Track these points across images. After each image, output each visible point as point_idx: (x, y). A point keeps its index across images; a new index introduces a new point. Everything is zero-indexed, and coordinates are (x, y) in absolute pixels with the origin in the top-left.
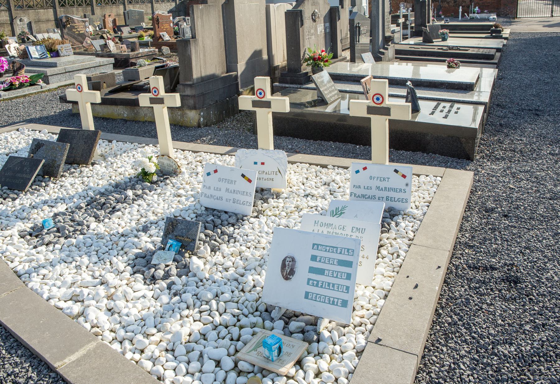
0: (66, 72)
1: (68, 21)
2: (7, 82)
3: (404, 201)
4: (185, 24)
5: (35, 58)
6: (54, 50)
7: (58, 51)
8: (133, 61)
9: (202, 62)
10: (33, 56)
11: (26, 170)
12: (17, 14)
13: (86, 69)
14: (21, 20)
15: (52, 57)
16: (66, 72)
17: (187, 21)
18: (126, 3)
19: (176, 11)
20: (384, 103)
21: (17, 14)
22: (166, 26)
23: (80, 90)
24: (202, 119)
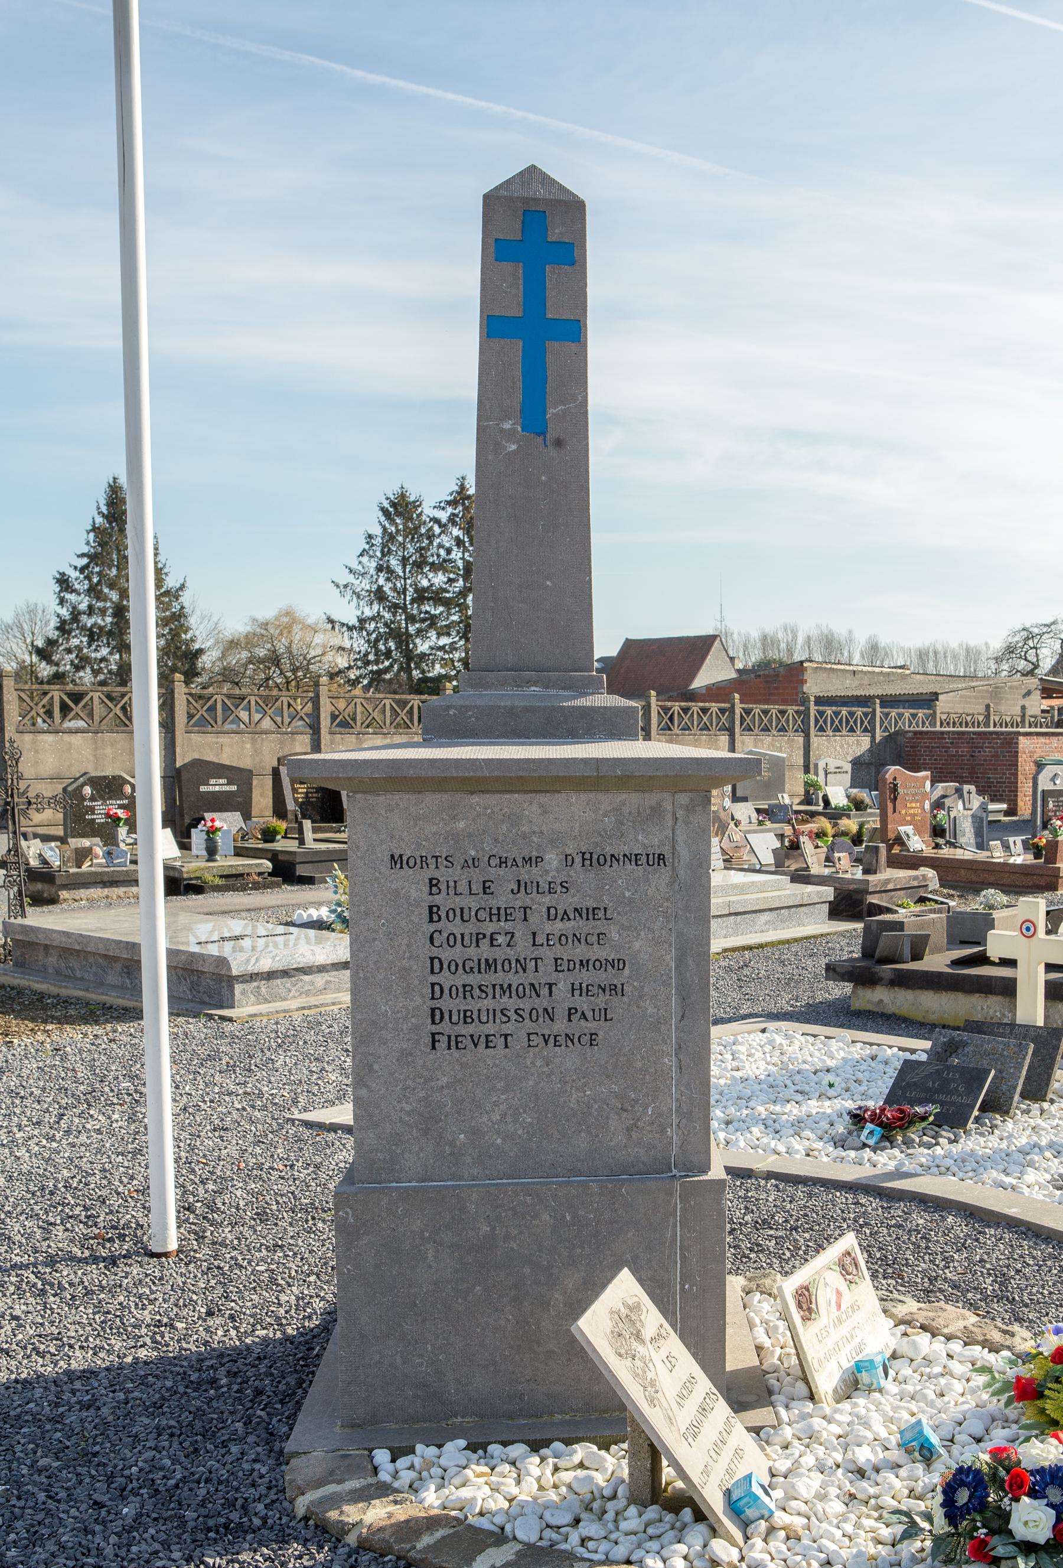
0: (730, 914)
4: (960, 806)
8: (874, 900)
11: (956, 1089)
13: (771, 910)
16: (730, 914)
17: (966, 795)
18: (737, 730)
19: (870, 764)
22: (914, 808)
23: (1030, 933)
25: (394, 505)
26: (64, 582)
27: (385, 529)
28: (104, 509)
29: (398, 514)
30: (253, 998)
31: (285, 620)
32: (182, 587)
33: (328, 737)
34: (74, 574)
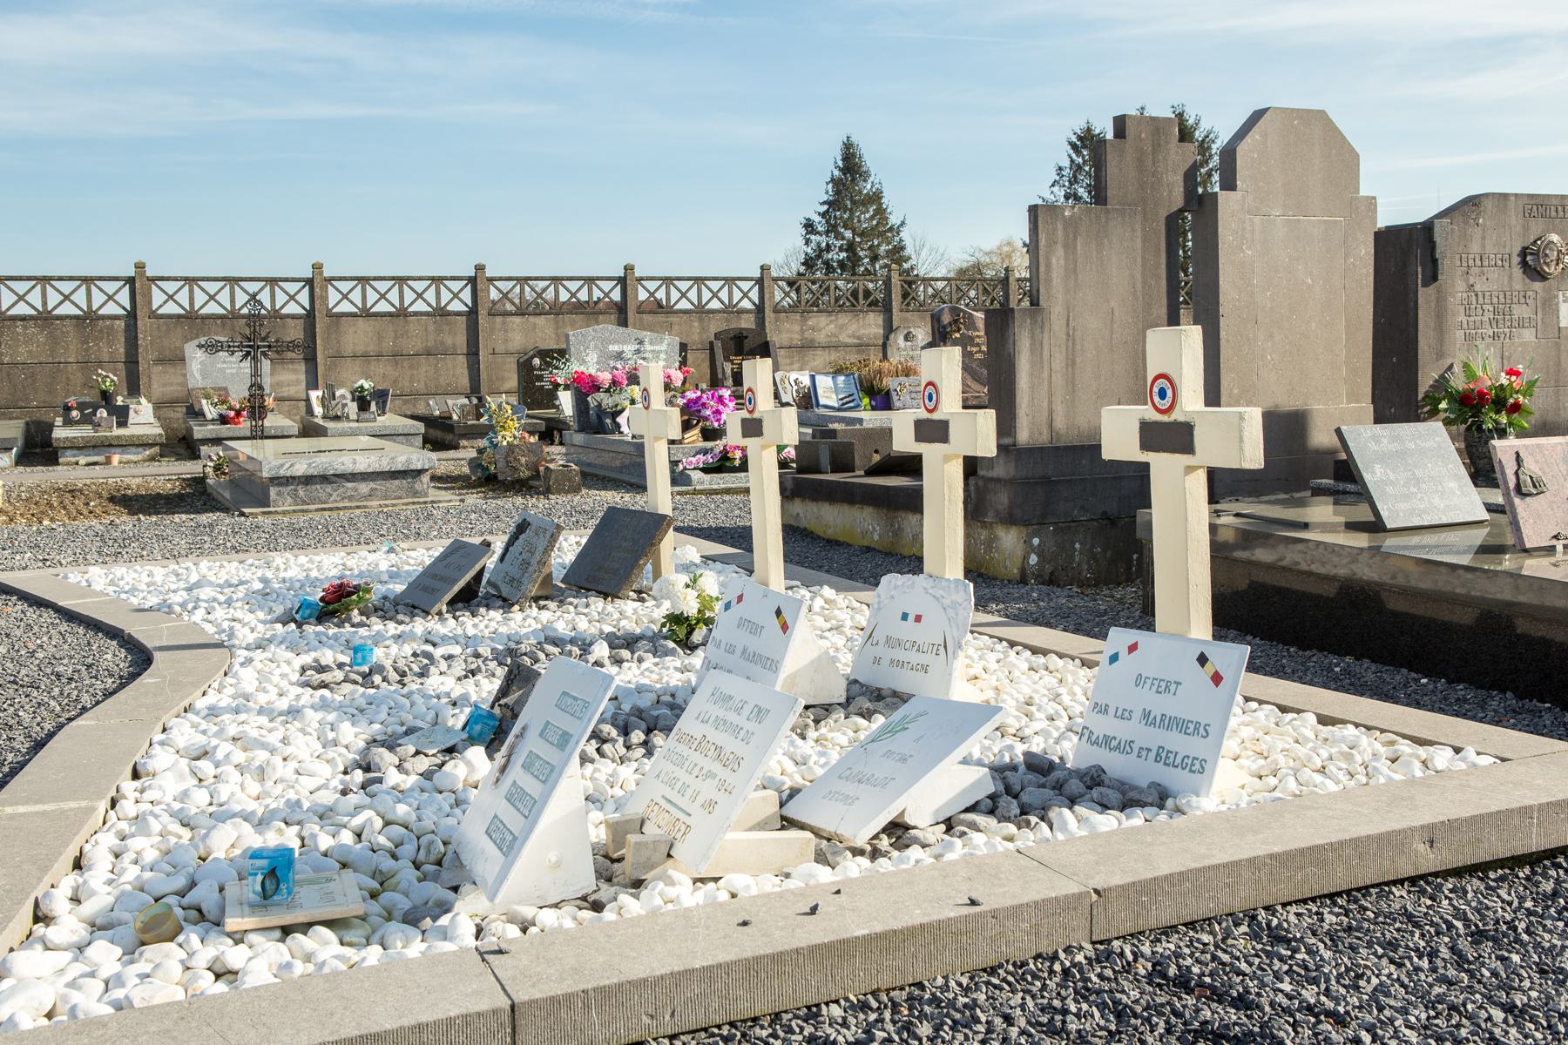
1: (956, 321)
2: (717, 451)
3: (1197, 766)
5: (826, 407)
6: (880, 391)
7: (888, 393)
9: (1058, 380)
10: (822, 401)
12: (906, 320)
14: (907, 338)
15: (873, 408)
20: (1177, 408)
21: (906, 320)
24: (1033, 559)
25: (1080, 138)
26: (809, 226)
27: (1072, 161)
28: (840, 164)
29: (1084, 146)
30: (289, 500)
31: (1006, 249)
32: (903, 223)
33: (773, 315)
34: (817, 219)
